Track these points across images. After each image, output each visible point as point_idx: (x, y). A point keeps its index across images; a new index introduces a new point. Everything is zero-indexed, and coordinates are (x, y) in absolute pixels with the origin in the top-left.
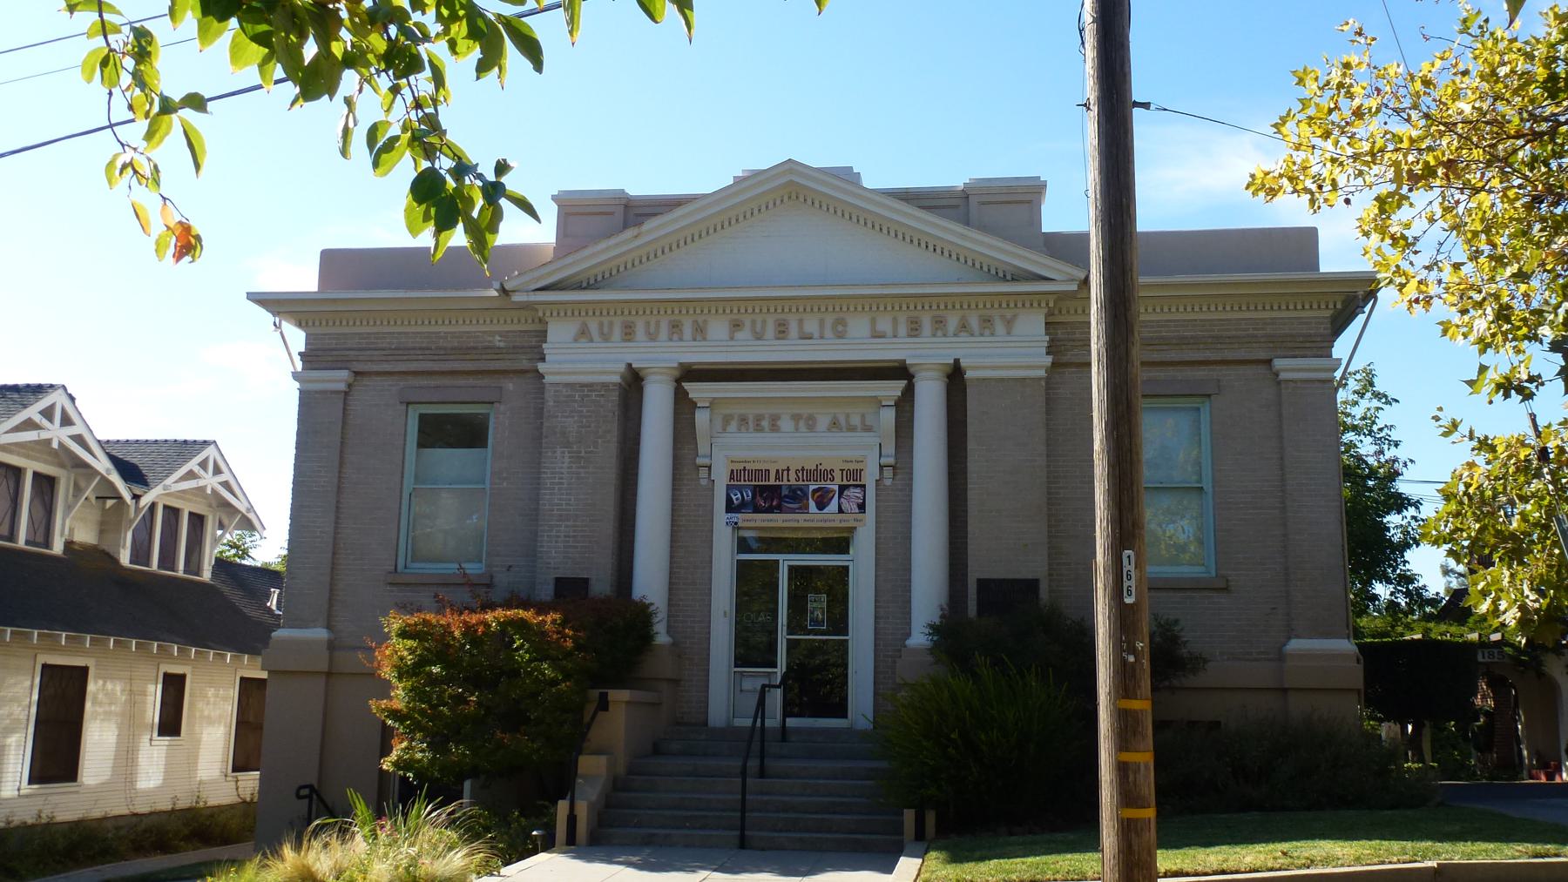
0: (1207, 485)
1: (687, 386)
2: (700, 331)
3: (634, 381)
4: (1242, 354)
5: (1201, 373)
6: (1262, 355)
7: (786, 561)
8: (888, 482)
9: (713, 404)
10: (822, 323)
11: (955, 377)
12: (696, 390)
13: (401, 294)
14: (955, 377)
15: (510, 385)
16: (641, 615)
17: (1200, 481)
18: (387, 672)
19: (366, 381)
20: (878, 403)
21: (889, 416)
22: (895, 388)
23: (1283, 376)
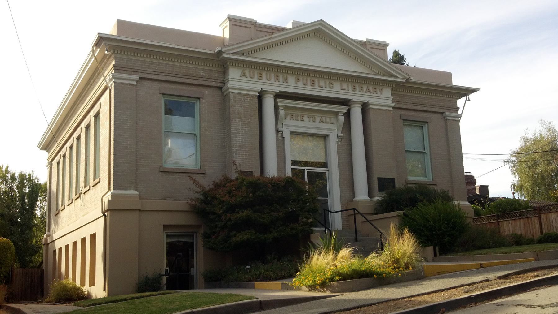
0: (197, 132)
1: (278, 100)
2: (286, 80)
3: (260, 97)
4: (437, 110)
5: (425, 115)
6: (441, 111)
7: (307, 169)
8: (339, 143)
9: (286, 108)
10: (325, 83)
11: (365, 107)
12: (282, 102)
13: (151, 49)
14: (365, 107)
15: (207, 92)
16: (382, 200)
17: (195, 131)
18: (244, 214)
19: (146, 83)
20: (337, 114)
21: (342, 118)
22: (344, 109)
23: (448, 118)
